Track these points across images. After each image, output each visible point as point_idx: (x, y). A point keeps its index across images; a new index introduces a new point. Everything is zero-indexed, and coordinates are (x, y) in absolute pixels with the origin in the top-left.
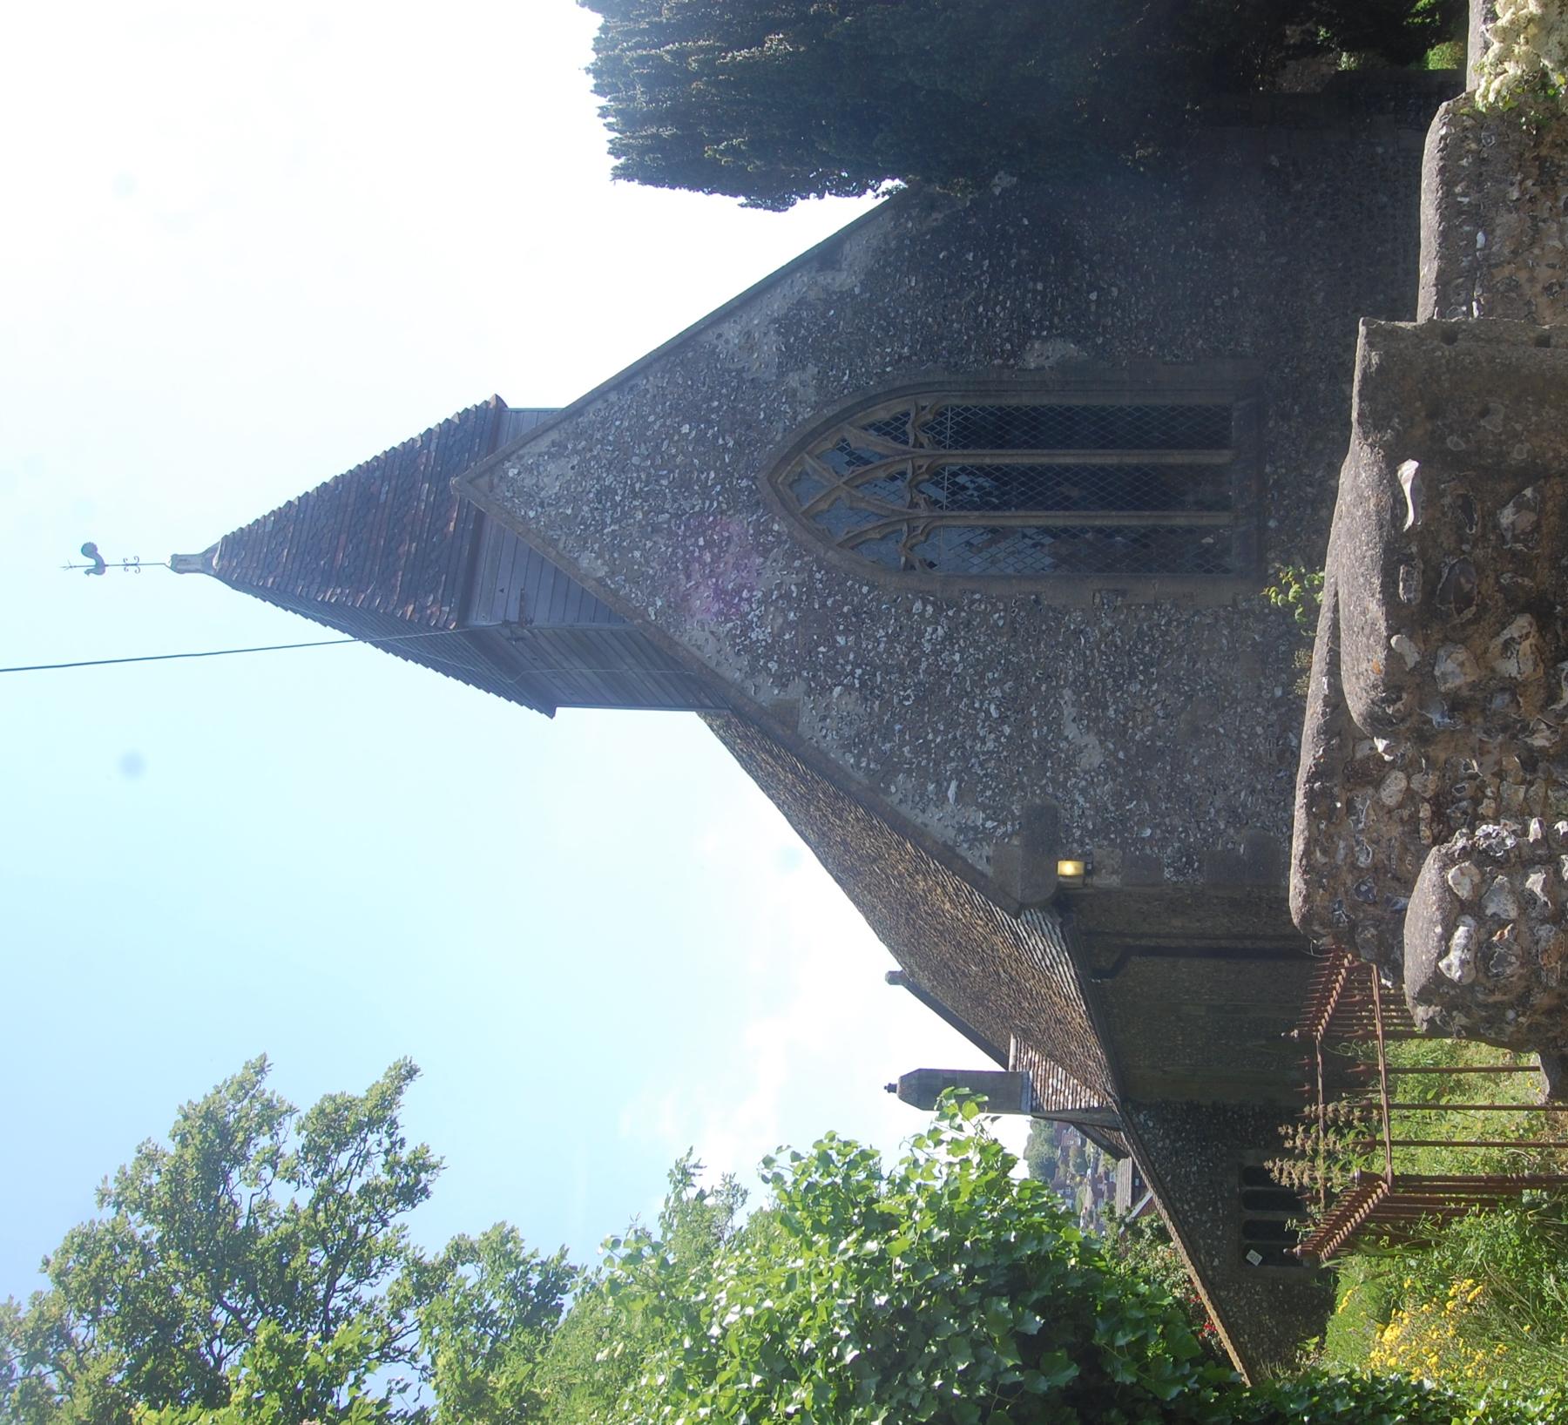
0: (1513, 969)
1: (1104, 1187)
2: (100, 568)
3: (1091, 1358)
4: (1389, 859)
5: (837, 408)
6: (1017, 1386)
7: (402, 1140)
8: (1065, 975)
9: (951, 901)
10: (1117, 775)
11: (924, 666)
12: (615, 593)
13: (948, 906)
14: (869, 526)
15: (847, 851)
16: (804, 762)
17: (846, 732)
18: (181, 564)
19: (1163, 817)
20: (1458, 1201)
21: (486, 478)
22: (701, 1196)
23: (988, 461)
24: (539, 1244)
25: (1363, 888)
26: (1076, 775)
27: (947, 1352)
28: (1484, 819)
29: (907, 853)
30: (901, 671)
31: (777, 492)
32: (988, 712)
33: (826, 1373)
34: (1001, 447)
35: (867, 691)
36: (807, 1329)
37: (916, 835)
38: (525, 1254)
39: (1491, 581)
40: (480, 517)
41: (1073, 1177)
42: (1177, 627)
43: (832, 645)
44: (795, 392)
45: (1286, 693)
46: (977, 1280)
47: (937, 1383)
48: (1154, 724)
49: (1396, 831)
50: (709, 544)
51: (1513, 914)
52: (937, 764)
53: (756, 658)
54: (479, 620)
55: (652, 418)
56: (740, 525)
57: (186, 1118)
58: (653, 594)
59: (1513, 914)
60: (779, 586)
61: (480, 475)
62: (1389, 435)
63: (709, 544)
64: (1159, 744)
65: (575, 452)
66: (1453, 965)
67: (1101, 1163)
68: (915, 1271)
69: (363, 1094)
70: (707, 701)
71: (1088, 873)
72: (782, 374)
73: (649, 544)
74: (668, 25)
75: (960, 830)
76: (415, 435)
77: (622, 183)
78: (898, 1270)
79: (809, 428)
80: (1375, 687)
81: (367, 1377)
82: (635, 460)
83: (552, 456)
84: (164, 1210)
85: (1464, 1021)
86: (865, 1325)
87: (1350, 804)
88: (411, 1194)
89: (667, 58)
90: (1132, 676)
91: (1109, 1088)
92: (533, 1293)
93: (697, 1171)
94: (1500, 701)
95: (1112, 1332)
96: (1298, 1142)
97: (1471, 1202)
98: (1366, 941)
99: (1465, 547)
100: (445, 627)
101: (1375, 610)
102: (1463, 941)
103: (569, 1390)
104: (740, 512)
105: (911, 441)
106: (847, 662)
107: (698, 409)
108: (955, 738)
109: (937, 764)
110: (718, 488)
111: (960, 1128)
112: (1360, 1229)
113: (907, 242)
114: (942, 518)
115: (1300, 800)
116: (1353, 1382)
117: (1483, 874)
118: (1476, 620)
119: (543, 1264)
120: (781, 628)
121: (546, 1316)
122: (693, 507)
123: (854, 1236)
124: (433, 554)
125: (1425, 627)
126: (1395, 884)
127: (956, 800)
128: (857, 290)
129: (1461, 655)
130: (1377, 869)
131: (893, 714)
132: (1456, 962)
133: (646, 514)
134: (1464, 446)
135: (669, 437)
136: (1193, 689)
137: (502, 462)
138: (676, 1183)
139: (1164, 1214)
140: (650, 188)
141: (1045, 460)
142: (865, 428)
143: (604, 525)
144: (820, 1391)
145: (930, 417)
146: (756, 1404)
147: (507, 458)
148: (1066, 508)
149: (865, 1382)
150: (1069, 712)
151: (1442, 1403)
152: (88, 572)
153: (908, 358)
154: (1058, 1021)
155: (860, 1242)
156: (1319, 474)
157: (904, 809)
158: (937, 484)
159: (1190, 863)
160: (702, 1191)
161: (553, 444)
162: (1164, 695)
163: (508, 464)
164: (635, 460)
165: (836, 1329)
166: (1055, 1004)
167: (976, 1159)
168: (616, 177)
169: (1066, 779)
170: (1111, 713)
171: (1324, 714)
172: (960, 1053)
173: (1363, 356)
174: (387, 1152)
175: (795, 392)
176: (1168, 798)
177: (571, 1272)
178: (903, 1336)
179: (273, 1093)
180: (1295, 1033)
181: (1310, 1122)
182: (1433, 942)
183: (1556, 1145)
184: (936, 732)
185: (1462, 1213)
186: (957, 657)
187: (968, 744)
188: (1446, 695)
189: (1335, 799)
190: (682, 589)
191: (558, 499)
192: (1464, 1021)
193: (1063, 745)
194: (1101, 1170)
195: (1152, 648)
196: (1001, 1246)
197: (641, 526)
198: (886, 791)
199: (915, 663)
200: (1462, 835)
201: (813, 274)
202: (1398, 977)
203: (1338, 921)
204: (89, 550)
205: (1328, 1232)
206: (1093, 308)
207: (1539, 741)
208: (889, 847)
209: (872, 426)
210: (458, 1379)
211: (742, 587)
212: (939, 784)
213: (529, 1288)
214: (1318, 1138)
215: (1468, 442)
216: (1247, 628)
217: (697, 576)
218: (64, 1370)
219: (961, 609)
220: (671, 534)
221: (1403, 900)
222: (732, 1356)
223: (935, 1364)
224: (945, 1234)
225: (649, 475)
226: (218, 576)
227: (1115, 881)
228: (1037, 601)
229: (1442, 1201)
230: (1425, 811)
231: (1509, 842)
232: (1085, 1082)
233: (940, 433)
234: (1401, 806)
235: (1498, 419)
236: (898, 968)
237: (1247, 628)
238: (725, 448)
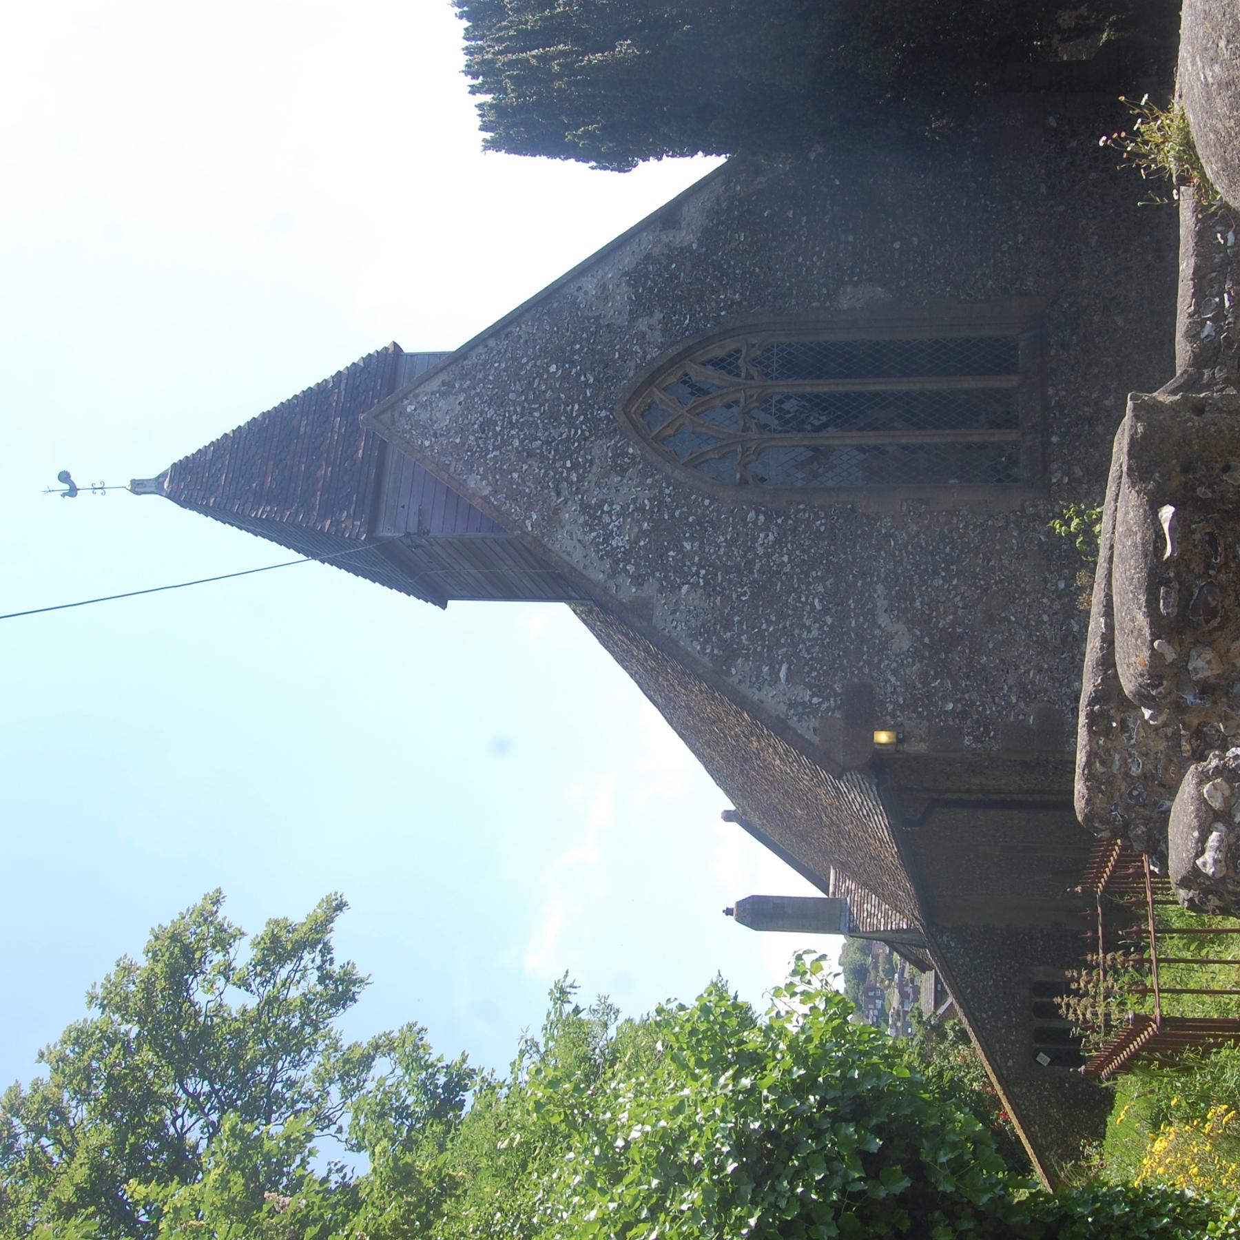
1: (909, 990)
2: (73, 491)
3: (918, 1170)
4: (1156, 768)
5: (680, 348)
6: (863, 1192)
7: (332, 959)
8: (880, 824)
9: (781, 759)
10: (923, 658)
11: (758, 566)
12: (498, 509)
13: (778, 762)
14: (710, 448)
15: (690, 713)
16: (655, 645)
17: (693, 623)
18: (138, 487)
19: (963, 693)
20: (1215, 1037)
21: (389, 414)
22: (577, 1011)
23: (808, 389)
24: (443, 1049)
25: (1135, 793)
26: (888, 657)
27: (806, 1166)
29: (744, 720)
30: (741, 575)
31: (630, 419)
32: (812, 605)
33: (711, 1179)
34: (818, 377)
35: (710, 588)
36: (696, 1144)
37: (756, 710)
38: (432, 1059)
39: (1232, 598)
40: (384, 446)
41: (882, 981)
42: (973, 530)
43: (680, 550)
44: (644, 335)
45: (1068, 586)
46: (828, 1108)
47: (799, 1190)
48: (955, 613)
49: (1162, 745)
50: (575, 466)
52: (770, 650)
53: (617, 562)
54: (386, 532)
55: (524, 360)
56: (601, 449)
57: (157, 938)
58: (530, 507)
61: (384, 412)
62: (1151, 485)
64: (959, 630)
65: (462, 390)
66: (1208, 862)
67: (907, 970)
68: (780, 1102)
70: (573, 594)
72: (632, 320)
73: (525, 467)
74: (533, 31)
75: (791, 706)
78: (766, 1101)
79: (656, 366)
80: (1142, 675)
81: (310, 1159)
82: (512, 396)
84: (139, 1014)
85: (1218, 903)
86: (742, 1144)
89: (534, 62)
90: (935, 573)
91: (916, 913)
92: (440, 1090)
93: (573, 990)
95: (935, 1150)
96: (1082, 985)
97: (1229, 1038)
98: (1138, 836)
99: (1211, 572)
100: (358, 538)
101: (1141, 619)
102: (1216, 844)
103: (475, 1171)
104: (600, 438)
105: (743, 374)
106: (693, 564)
107: (564, 352)
108: (785, 627)
109: (770, 650)
110: (582, 418)
111: (809, 983)
112: (1135, 1056)
113: (737, 203)
114: (771, 439)
115: (1082, 720)
116: (1128, 1190)
117: (1232, 788)
118: (1221, 627)
119: (448, 1067)
120: (637, 535)
121: (453, 1110)
122: (561, 435)
123: (730, 1072)
124: (342, 476)
125: (1181, 633)
126: (1161, 790)
127: (787, 680)
128: (695, 246)
129: (1209, 655)
131: (732, 608)
132: (1210, 861)
133: (521, 442)
134: (1210, 495)
135: (540, 376)
136: (987, 583)
137: (401, 400)
139: (965, 1020)
140: (513, 156)
141: (857, 388)
142: (703, 364)
144: (707, 1194)
145: (759, 353)
146: (654, 1200)
148: (876, 429)
149: (743, 1188)
150: (882, 604)
151: (1201, 1208)
152: (64, 495)
153: (740, 303)
155: (736, 1078)
156: (1095, 395)
157: (744, 688)
158: (765, 410)
159: (987, 732)
160: (577, 1007)
161: (443, 384)
162: (963, 588)
163: (406, 402)
164: (512, 396)
165: (718, 1145)
166: (870, 844)
167: (822, 1007)
168: (486, 148)
169: (880, 661)
170: (918, 604)
171: (1102, 649)
172: (789, 883)
174: (319, 968)
175: (644, 335)
176: (968, 677)
177: (471, 1074)
178: (771, 1151)
179: (225, 918)
180: (1079, 889)
181: (1091, 967)
182: (1191, 844)
184: (769, 623)
185: (1220, 1046)
186: (785, 559)
187: (796, 632)
189: (1111, 719)
190: (553, 504)
191: (448, 431)
192: (1218, 903)
193: (877, 632)
194: (906, 975)
195: (952, 549)
196: (848, 1082)
197: (518, 452)
198: (728, 672)
199: (750, 563)
200: (1215, 756)
201: (657, 233)
202: (1163, 860)
203: (1115, 820)
204: (64, 477)
205: (1107, 1058)
206: (897, 255)
208: (728, 714)
209: (710, 361)
210: (392, 1165)
211: (604, 502)
212: (772, 667)
213: (437, 1087)
214: (1098, 980)
215: (1213, 492)
216: (1034, 530)
217: (565, 493)
218: (61, 1144)
219: (787, 518)
220: (543, 458)
221: (1167, 803)
222: (634, 1162)
223: (796, 1175)
224: (802, 1072)
225: (523, 408)
227: (922, 748)
228: (853, 510)
229: (1203, 1037)
232: (895, 908)
233: (767, 366)
236: (732, 808)
237: (1034, 530)
238: (586, 383)
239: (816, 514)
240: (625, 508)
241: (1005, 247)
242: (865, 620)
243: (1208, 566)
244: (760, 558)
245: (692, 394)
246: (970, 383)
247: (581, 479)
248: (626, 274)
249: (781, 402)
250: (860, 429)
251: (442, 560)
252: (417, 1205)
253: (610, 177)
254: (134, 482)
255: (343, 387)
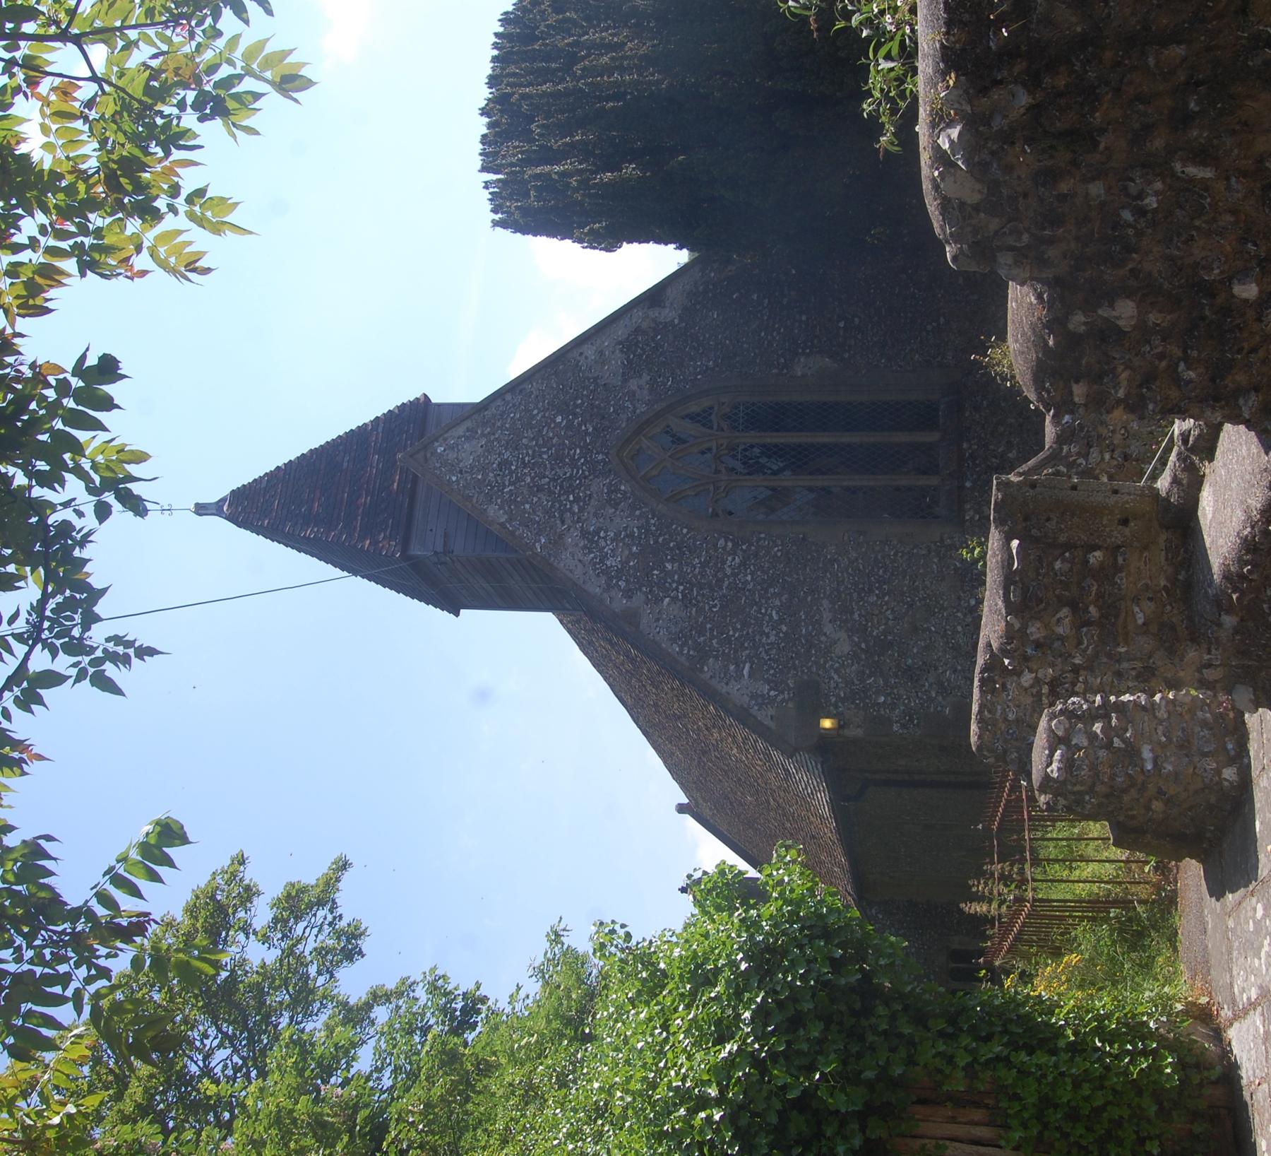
0: (1085, 772)
8: (822, 801)
9: (738, 747)
11: (726, 583)
12: (512, 533)
15: (657, 712)
18: (201, 509)
23: (769, 440)
28: (1077, 694)
32: (771, 616)
34: (777, 430)
38: (450, 988)
40: (415, 480)
43: (663, 569)
44: (634, 393)
49: (1029, 700)
50: (577, 500)
51: (1086, 744)
52: (736, 651)
53: (610, 579)
54: (416, 551)
57: (197, 897)
58: (539, 534)
59: (1086, 744)
60: (625, 529)
63: (577, 500)
65: (483, 435)
68: (775, 926)
69: (313, 882)
71: (841, 726)
72: (625, 381)
76: (367, 421)
77: (498, 229)
82: (525, 441)
83: (468, 439)
85: (1064, 802)
87: (1004, 686)
88: (351, 953)
90: (871, 591)
91: (849, 888)
94: (1057, 644)
100: (393, 555)
109: (736, 651)
115: (976, 683)
118: (1045, 609)
119: (464, 994)
127: (750, 676)
128: (676, 321)
130: (1018, 721)
133: (533, 479)
135: (548, 425)
137: (432, 442)
138: (551, 941)
143: (504, 487)
147: (437, 440)
148: (824, 473)
154: (813, 837)
158: (733, 457)
159: (911, 720)
161: (468, 430)
162: (893, 604)
164: (525, 441)
166: (811, 823)
170: (856, 616)
173: (995, 495)
175: (634, 393)
176: (896, 676)
177: (484, 1000)
180: (980, 827)
182: (1044, 759)
183: (1130, 883)
184: (735, 630)
186: (749, 578)
187: (757, 638)
188: (1033, 641)
189: (995, 682)
191: (472, 468)
192: (1064, 802)
193: (823, 638)
195: (885, 572)
198: (701, 670)
199: (720, 581)
207: (1077, 661)
209: (687, 416)
212: (737, 666)
217: (568, 522)
220: (551, 493)
226: (229, 518)
227: (859, 732)
228: (803, 539)
230: (1045, 690)
231: (1085, 707)
233: (735, 421)
234: (1032, 686)
235: (1054, 522)
236: (686, 801)
239: (774, 542)
240: (617, 534)
241: (929, 327)
242: (814, 629)
243: (1038, 574)
244: (728, 577)
245: (673, 442)
246: (901, 437)
247: (581, 510)
248: (620, 343)
249: (745, 450)
250: (811, 474)
251: (456, 572)
252: (460, 1082)
253: (598, 255)
254: (197, 505)
255: (380, 430)
